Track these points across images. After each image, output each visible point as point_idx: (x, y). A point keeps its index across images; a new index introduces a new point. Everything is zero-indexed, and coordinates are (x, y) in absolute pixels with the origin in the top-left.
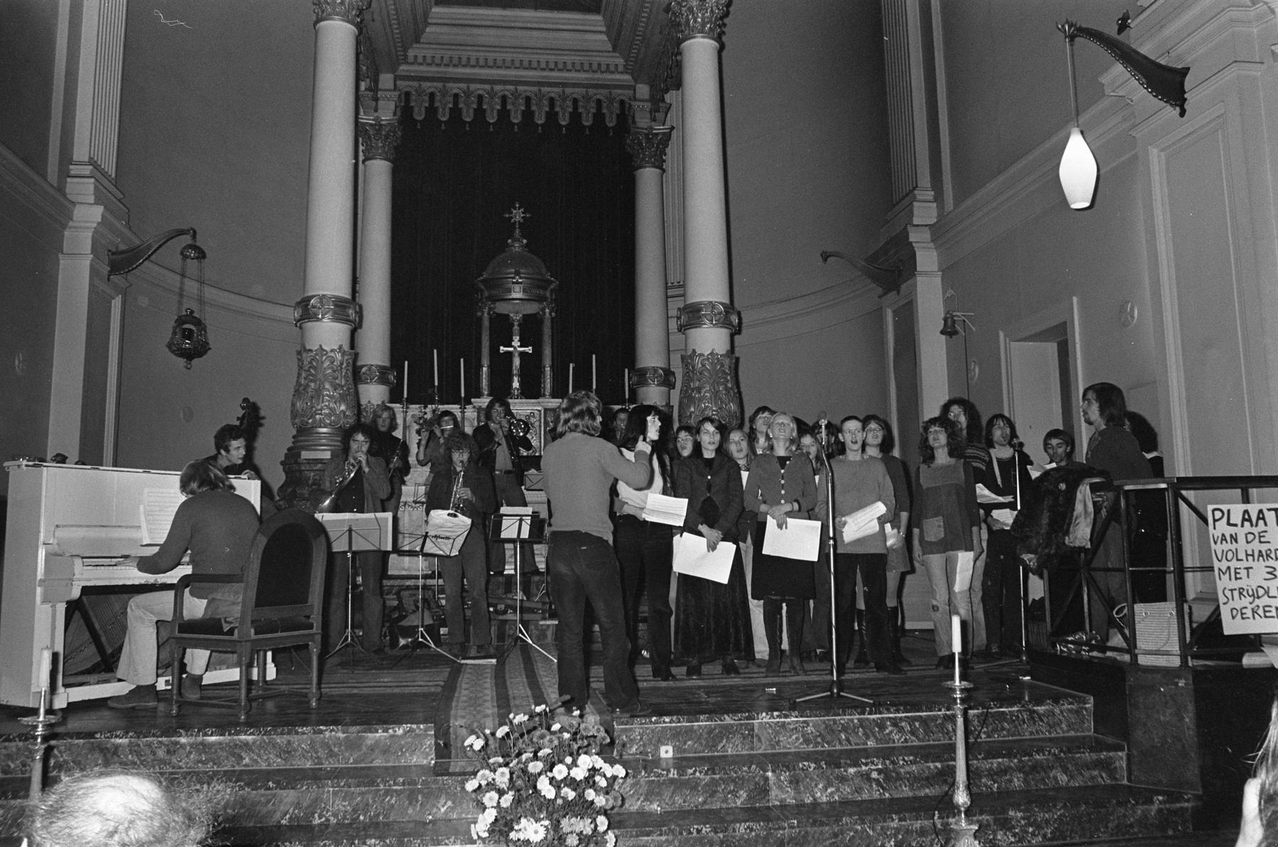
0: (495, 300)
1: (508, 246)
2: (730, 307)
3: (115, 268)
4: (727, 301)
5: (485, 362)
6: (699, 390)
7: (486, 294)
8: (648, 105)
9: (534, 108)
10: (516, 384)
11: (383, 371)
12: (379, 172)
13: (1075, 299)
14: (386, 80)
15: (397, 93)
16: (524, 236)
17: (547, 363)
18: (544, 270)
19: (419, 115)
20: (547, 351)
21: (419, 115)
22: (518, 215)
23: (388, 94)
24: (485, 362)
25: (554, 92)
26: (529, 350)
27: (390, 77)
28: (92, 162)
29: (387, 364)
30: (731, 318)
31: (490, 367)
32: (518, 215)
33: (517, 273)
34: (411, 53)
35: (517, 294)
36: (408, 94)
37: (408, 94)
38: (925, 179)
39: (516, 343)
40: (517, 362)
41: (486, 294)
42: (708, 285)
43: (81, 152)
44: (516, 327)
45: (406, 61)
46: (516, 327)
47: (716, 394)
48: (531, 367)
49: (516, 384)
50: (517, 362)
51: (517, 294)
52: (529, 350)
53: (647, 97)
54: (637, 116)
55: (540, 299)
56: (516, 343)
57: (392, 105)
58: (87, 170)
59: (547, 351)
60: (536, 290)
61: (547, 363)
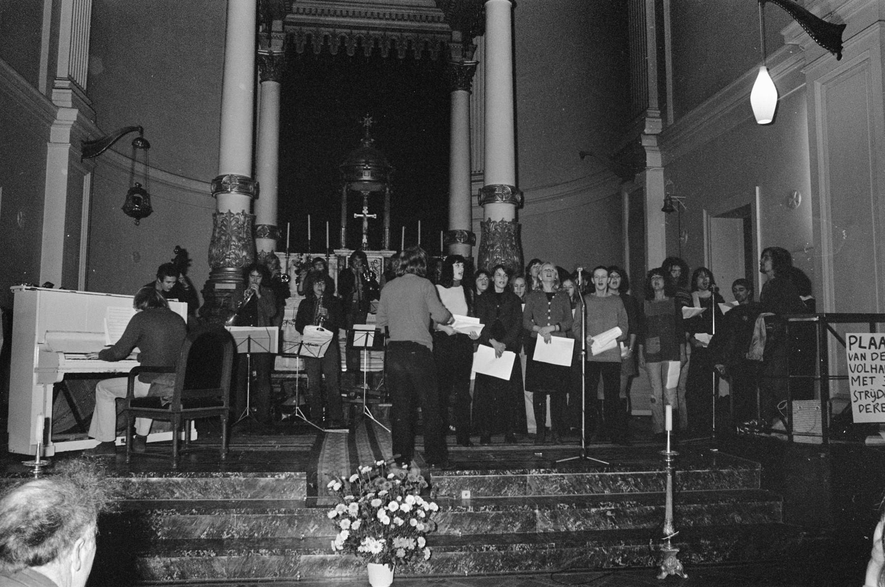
0: (352, 181)
1: (360, 142)
2: (515, 190)
4: (513, 184)
5: (344, 224)
6: (492, 246)
10: (365, 240)
12: (271, 88)
14: (277, 25)
20: (387, 219)
22: (368, 122)
23: (278, 35)
25: (395, 35)
26: (374, 216)
27: (279, 22)
29: (275, 224)
30: (516, 196)
33: (367, 163)
35: (367, 177)
38: (654, 102)
39: (365, 211)
40: (366, 224)
43: (62, 71)
47: (504, 249)
48: (376, 227)
49: (365, 240)
50: (366, 224)
51: (367, 177)
52: (374, 216)
56: (365, 211)
57: (281, 43)
58: (67, 84)
59: (387, 219)
60: (378, 177)
61: (387, 225)
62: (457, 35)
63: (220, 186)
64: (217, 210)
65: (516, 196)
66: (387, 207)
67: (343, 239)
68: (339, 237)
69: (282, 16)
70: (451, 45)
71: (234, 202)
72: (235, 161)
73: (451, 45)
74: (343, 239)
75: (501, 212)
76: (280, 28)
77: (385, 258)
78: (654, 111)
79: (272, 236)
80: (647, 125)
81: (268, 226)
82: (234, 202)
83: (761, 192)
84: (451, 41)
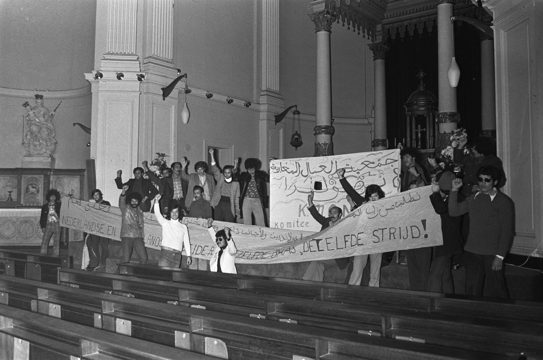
57: (381, 37)
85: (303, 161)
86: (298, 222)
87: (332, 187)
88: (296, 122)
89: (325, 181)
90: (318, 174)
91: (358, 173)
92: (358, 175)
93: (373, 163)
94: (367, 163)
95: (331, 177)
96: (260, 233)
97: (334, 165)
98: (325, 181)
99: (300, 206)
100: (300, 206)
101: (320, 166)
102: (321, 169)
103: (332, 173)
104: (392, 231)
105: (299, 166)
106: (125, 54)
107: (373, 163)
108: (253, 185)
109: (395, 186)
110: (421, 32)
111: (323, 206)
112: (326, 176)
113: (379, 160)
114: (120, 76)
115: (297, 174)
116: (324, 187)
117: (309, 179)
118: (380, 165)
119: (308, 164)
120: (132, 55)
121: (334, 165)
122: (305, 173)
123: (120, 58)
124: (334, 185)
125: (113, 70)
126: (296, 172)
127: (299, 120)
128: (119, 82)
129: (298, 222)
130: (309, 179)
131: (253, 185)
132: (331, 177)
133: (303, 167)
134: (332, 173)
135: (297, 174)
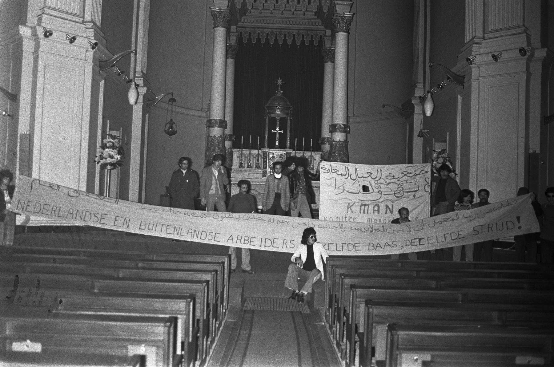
0: (270, 113)
1: (276, 93)
2: (346, 126)
3: (101, 67)
4: (345, 123)
5: (267, 135)
6: (334, 153)
7: (267, 111)
8: (330, 38)
9: (287, 38)
10: (277, 144)
11: (230, 136)
12: (230, 61)
13: (448, 133)
14: (233, 28)
15: (237, 34)
16: (281, 90)
17: (288, 136)
18: (288, 103)
19: (245, 41)
20: (288, 133)
21: (245, 41)
22: (280, 82)
23: (234, 34)
24: (267, 135)
25: (295, 32)
26: (282, 131)
27: (235, 27)
28: (92, 21)
29: (232, 133)
30: (346, 129)
31: (268, 137)
32: (280, 82)
33: (279, 105)
34: (242, 19)
35: (278, 112)
36: (241, 33)
37: (241, 33)
38: (421, 80)
39: (278, 129)
40: (278, 136)
41: (267, 111)
42: (340, 120)
43: (138, 69)
44: (278, 122)
45: (240, 21)
46: (278, 122)
47: (339, 154)
48: (282, 137)
49: (277, 144)
50: (278, 136)
51: (278, 112)
52: (282, 131)
53: (337, 6)
54: (326, 43)
55: (287, 114)
56: (278, 129)
57: (235, 38)
58: (141, 75)
59: (288, 133)
60: (285, 110)
61: (288, 136)
62: (328, 32)
63: (210, 124)
64: (209, 135)
65: (346, 129)
66: (288, 128)
67: (266, 143)
68: (264, 142)
69: (236, 24)
70: (324, 37)
71: (216, 131)
72: (216, 113)
73: (324, 37)
74: (266, 143)
75: (339, 137)
76: (235, 31)
77: (287, 153)
78: (420, 85)
79: (230, 140)
80: (416, 92)
81: (229, 135)
82: (216, 131)
83: (449, 135)
84: (325, 36)
85: (352, 166)
86: (346, 217)
87: (377, 190)
88: (169, 113)
89: (371, 185)
90: (364, 179)
91: (398, 180)
92: (398, 182)
93: (411, 173)
94: (405, 173)
95: (376, 182)
96: (339, 227)
97: (379, 173)
98: (371, 185)
99: (349, 204)
100: (349, 204)
101: (367, 173)
102: (368, 175)
103: (377, 179)
104: (247, 238)
105: (348, 170)
106: (67, 13)
107: (411, 173)
108: (301, 185)
109: (426, 191)
110: (263, 42)
111: (368, 205)
112: (372, 181)
113: (415, 171)
114: (72, 40)
115: (347, 176)
116: (371, 190)
117: (357, 182)
118: (416, 175)
119: (356, 169)
120: (75, 15)
121: (379, 173)
122: (354, 177)
123: (139, 36)
124: (380, 189)
125: (85, 35)
126: (345, 175)
127: (172, 111)
128: (70, 47)
129: (346, 217)
130: (357, 182)
131: (301, 185)
132: (376, 182)
133: (352, 171)
134: (377, 179)
135: (347, 176)
